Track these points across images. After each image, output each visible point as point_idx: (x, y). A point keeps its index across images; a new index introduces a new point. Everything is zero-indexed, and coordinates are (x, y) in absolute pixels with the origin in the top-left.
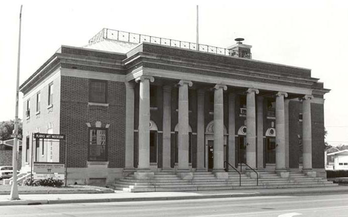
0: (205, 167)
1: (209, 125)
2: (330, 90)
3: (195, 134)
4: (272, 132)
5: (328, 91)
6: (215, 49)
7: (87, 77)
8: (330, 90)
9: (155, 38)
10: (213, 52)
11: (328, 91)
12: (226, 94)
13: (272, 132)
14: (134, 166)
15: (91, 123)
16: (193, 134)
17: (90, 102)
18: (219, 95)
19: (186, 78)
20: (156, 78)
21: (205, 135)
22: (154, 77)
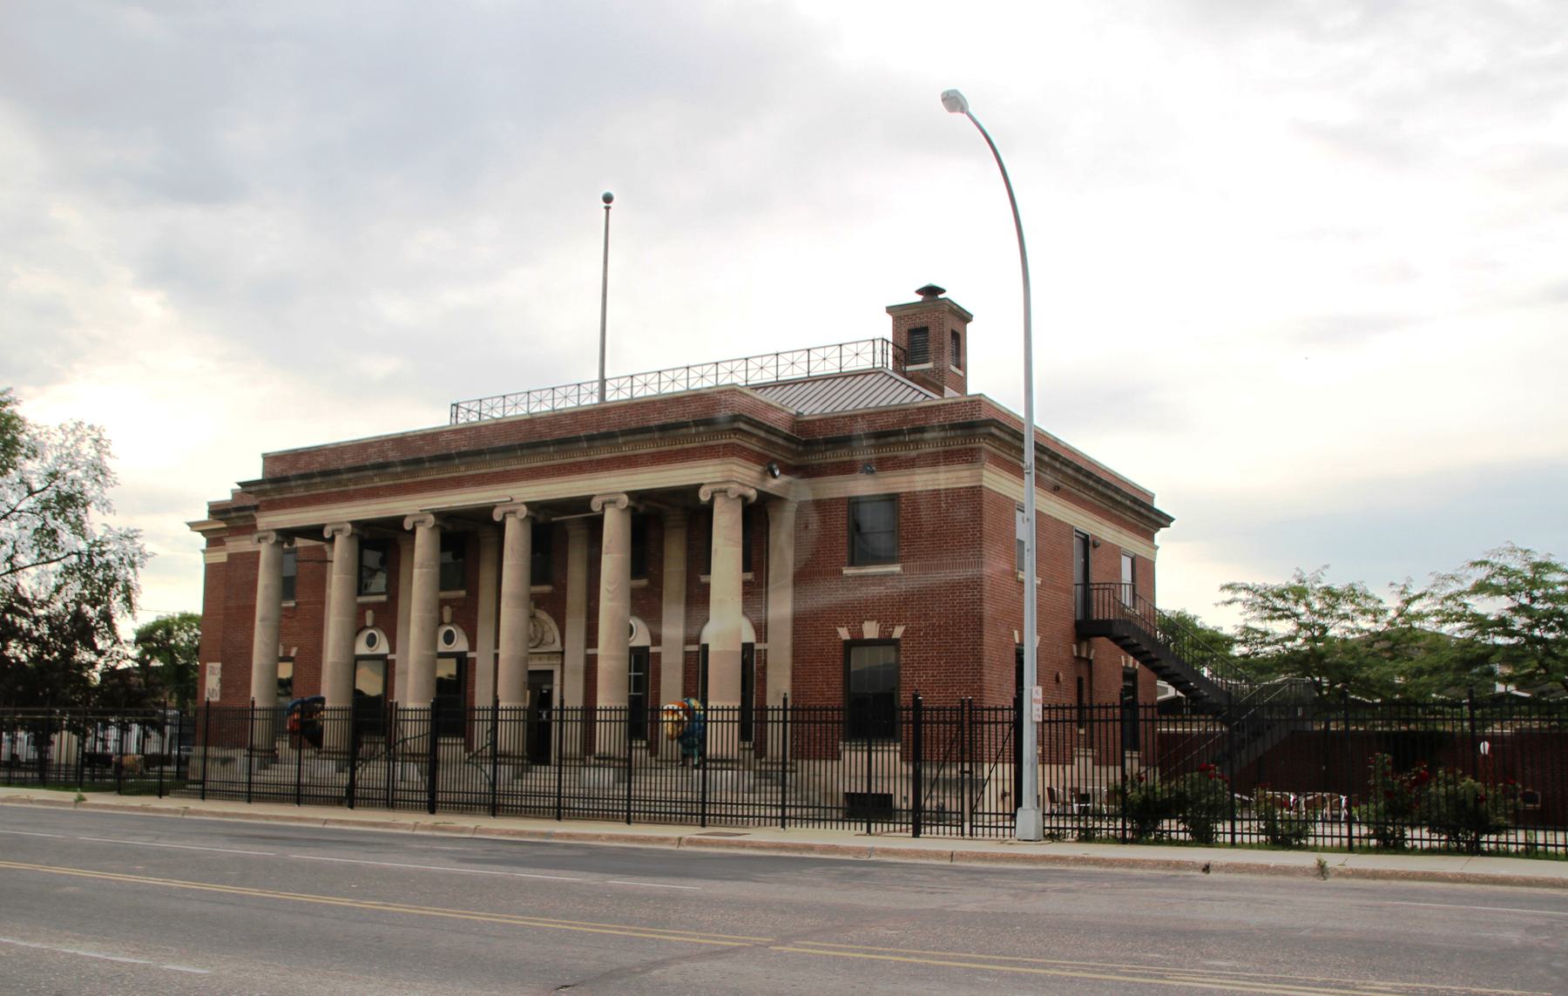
20: (636, 496)
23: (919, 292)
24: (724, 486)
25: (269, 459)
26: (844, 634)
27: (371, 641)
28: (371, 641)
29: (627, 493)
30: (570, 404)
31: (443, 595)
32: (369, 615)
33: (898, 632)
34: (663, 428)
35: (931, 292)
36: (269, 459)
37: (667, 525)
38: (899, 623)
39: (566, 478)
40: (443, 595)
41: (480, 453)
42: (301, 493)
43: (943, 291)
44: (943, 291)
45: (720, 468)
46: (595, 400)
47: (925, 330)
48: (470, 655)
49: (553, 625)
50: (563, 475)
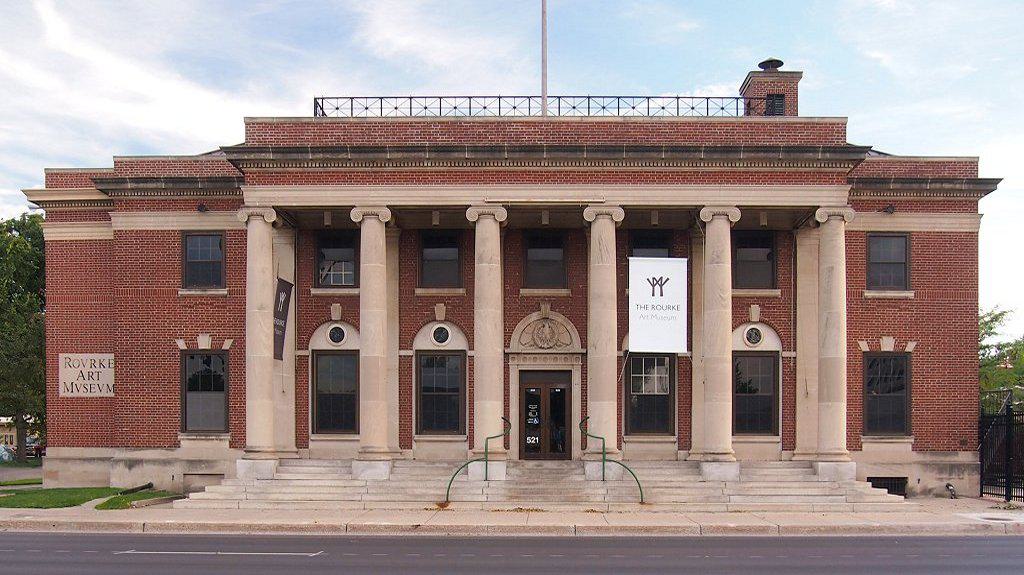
0: (507, 445)
1: (520, 326)
2: (999, 180)
3: (793, 354)
4: (337, 335)
5: (990, 185)
6: (645, 104)
7: (175, 228)
8: (999, 180)
9: (511, 100)
10: (695, 114)
11: (990, 185)
12: (507, 233)
13: (337, 335)
14: (298, 445)
15: (186, 339)
16: (786, 354)
17: (523, 288)
18: (488, 242)
19: (488, 204)
20: (511, 209)
21: (506, 355)
22: (273, 207)
23: (761, 65)
24: (375, 210)
25: (251, 124)
26: (181, 344)
27: (441, 336)
28: (441, 336)
29: (623, 207)
30: (670, 112)
31: (354, 291)
32: (755, 311)
33: (910, 347)
34: (789, 150)
35: (771, 65)
36: (251, 124)
37: (547, 247)
38: (911, 339)
39: (472, 186)
40: (354, 291)
41: (617, 149)
42: (316, 168)
43: (780, 63)
44: (780, 63)
45: (835, 194)
46: (540, 114)
47: (782, 97)
48: (469, 353)
49: (570, 326)
50: (468, 181)
